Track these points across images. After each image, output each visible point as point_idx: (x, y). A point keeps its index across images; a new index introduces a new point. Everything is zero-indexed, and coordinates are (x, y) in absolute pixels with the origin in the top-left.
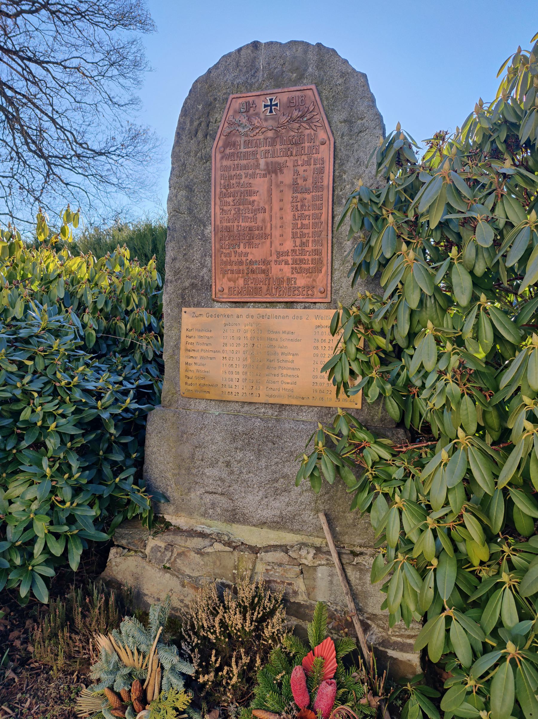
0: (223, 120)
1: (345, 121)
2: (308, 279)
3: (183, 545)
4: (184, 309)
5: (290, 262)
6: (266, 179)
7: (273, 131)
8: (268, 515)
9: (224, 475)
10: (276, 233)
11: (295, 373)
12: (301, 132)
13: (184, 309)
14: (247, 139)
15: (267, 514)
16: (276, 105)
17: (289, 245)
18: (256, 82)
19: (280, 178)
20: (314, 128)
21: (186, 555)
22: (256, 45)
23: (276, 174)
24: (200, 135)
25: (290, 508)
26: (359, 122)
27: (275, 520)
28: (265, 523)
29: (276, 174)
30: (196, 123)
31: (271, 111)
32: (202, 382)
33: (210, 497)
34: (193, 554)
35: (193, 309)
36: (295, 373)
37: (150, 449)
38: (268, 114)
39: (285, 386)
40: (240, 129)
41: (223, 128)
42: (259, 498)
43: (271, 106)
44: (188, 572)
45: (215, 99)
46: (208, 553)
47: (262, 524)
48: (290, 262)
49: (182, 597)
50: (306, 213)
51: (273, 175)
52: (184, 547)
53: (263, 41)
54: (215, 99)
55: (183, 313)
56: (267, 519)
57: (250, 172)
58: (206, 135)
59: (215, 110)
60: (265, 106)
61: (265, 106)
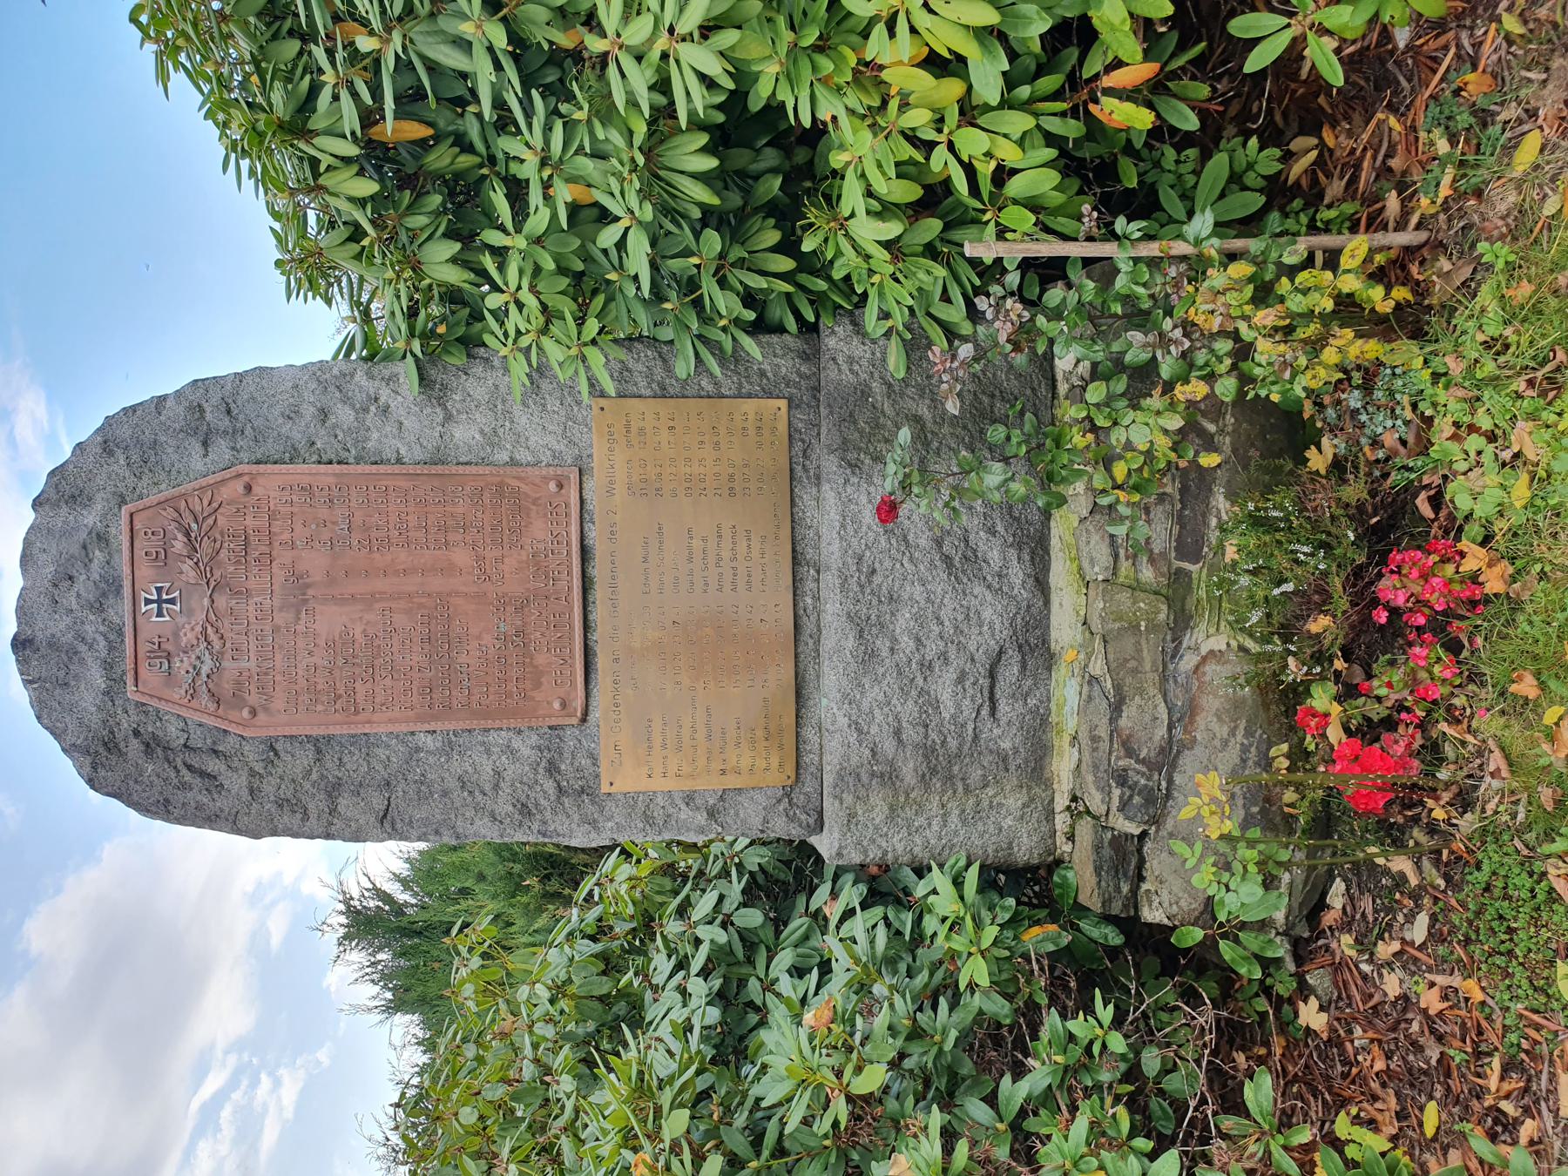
0: (182, 715)
1: (205, 444)
2: (533, 514)
3: (1107, 743)
4: (605, 788)
5: (497, 553)
6: (319, 608)
7: (215, 596)
8: (1021, 574)
9: (950, 675)
10: (437, 583)
11: (727, 588)
12: (222, 534)
13: (605, 788)
14: (228, 656)
15: (1017, 574)
16: (159, 590)
17: (462, 557)
18: (106, 639)
19: (317, 576)
20: (215, 505)
21: (1130, 736)
22: (21, 644)
23: (308, 586)
24: (213, 765)
25: (1000, 528)
26: (209, 416)
27: (1027, 558)
28: (1037, 580)
29: (308, 586)
30: (187, 776)
31: (172, 601)
32: (760, 733)
33: (1003, 707)
34: (1123, 722)
35: (603, 770)
36: (727, 588)
37: (917, 850)
38: (177, 608)
39: (755, 553)
40: (205, 670)
41: (202, 715)
42: (987, 593)
43: (159, 601)
44: (1161, 732)
45: (136, 733)
46: (1118, 688)
47: (1041, 585)
48: (497, 553)
49: (1217, 743)
50: (393, 518)
51: (311, 592)
52: (1111, 741)
53: (12, 628)
54: (136, 733)
55: (613, 790)
56: (1029, 576)
57: (301, 643)
58: (215, 752)
59: (161, 734)
60: (160, 614)
61: (160, 614)
